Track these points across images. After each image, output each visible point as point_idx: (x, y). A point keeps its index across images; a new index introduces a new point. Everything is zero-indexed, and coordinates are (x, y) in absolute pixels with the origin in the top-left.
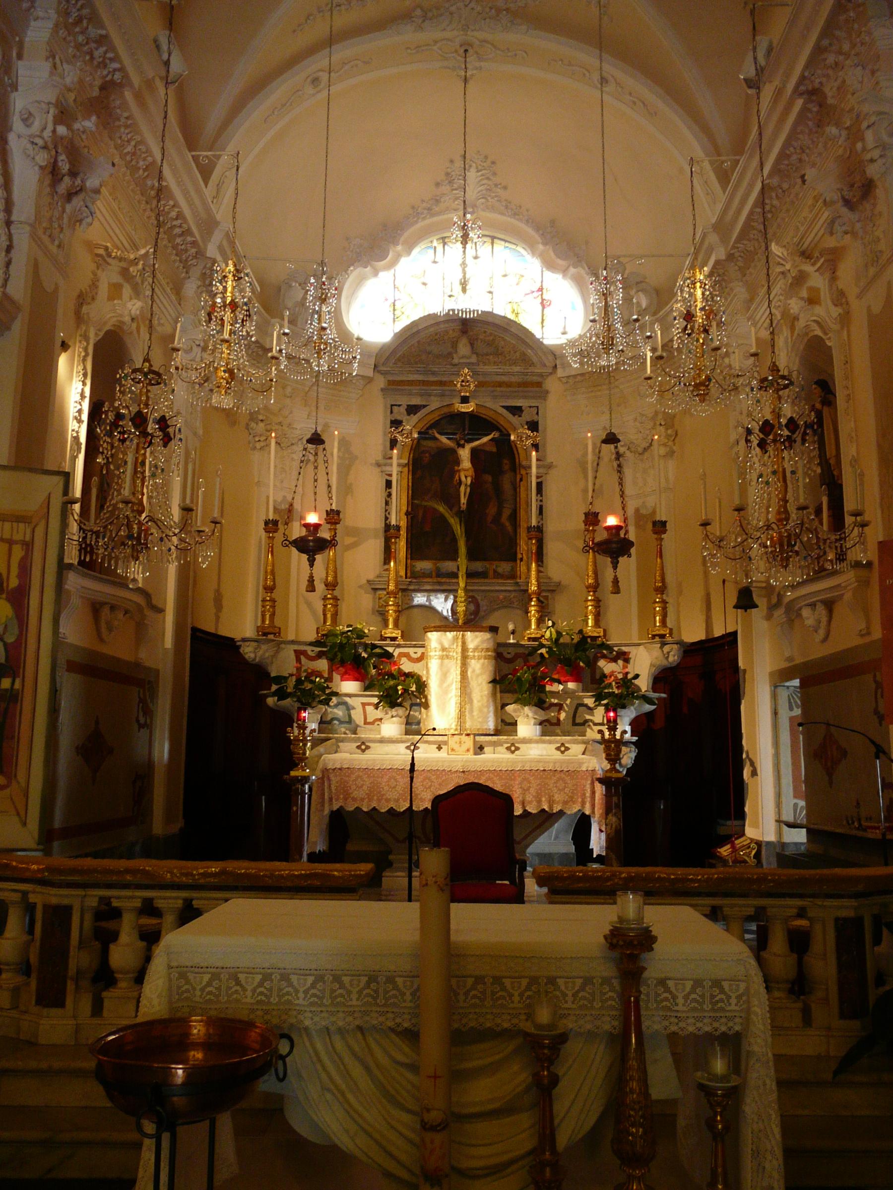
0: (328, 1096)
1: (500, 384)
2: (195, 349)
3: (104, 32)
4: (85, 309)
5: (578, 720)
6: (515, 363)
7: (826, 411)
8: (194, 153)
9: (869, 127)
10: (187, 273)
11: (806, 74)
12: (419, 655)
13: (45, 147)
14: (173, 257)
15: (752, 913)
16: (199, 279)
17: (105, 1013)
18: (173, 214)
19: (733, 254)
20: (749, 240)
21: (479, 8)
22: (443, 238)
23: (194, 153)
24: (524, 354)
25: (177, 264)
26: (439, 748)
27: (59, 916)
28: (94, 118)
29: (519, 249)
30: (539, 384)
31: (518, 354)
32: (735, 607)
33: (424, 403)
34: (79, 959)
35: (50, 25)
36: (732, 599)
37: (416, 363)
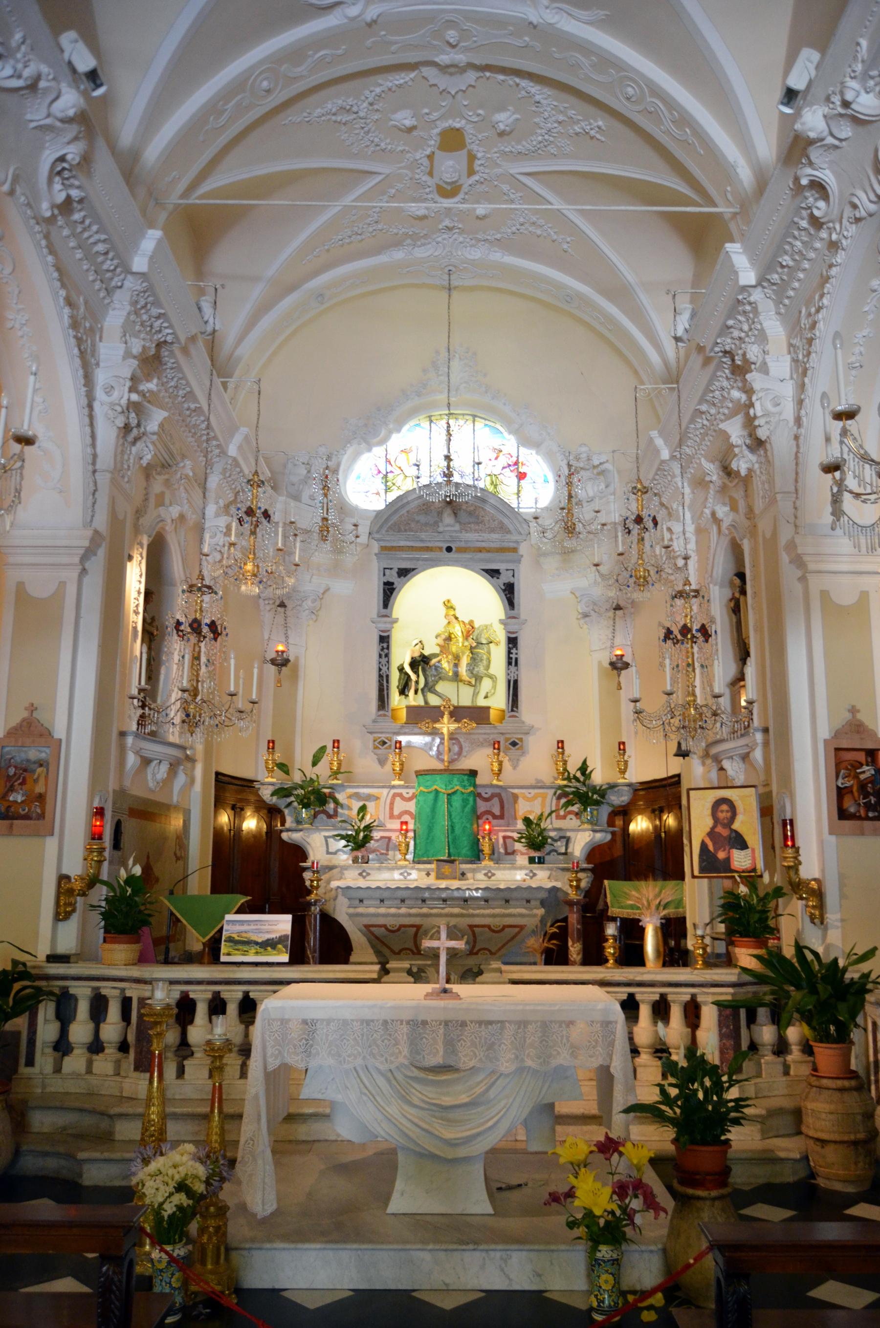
0: (365, 1098)
1: (480, 550)
3: (163, 311)
4: (141, 521)
6: (492, 531)
7: (742, 598)
12: (410, 795)
13: (123, 412)
17: (186, 1076)
21: (461, 239)
22: (430, 417)
24: (501, 523)
26: (428, 874)
28: (155, 381)
29: (498, 426)
30: (515, 550)
32: (676, 755)
35: (125, 313)
37: (406, 531)
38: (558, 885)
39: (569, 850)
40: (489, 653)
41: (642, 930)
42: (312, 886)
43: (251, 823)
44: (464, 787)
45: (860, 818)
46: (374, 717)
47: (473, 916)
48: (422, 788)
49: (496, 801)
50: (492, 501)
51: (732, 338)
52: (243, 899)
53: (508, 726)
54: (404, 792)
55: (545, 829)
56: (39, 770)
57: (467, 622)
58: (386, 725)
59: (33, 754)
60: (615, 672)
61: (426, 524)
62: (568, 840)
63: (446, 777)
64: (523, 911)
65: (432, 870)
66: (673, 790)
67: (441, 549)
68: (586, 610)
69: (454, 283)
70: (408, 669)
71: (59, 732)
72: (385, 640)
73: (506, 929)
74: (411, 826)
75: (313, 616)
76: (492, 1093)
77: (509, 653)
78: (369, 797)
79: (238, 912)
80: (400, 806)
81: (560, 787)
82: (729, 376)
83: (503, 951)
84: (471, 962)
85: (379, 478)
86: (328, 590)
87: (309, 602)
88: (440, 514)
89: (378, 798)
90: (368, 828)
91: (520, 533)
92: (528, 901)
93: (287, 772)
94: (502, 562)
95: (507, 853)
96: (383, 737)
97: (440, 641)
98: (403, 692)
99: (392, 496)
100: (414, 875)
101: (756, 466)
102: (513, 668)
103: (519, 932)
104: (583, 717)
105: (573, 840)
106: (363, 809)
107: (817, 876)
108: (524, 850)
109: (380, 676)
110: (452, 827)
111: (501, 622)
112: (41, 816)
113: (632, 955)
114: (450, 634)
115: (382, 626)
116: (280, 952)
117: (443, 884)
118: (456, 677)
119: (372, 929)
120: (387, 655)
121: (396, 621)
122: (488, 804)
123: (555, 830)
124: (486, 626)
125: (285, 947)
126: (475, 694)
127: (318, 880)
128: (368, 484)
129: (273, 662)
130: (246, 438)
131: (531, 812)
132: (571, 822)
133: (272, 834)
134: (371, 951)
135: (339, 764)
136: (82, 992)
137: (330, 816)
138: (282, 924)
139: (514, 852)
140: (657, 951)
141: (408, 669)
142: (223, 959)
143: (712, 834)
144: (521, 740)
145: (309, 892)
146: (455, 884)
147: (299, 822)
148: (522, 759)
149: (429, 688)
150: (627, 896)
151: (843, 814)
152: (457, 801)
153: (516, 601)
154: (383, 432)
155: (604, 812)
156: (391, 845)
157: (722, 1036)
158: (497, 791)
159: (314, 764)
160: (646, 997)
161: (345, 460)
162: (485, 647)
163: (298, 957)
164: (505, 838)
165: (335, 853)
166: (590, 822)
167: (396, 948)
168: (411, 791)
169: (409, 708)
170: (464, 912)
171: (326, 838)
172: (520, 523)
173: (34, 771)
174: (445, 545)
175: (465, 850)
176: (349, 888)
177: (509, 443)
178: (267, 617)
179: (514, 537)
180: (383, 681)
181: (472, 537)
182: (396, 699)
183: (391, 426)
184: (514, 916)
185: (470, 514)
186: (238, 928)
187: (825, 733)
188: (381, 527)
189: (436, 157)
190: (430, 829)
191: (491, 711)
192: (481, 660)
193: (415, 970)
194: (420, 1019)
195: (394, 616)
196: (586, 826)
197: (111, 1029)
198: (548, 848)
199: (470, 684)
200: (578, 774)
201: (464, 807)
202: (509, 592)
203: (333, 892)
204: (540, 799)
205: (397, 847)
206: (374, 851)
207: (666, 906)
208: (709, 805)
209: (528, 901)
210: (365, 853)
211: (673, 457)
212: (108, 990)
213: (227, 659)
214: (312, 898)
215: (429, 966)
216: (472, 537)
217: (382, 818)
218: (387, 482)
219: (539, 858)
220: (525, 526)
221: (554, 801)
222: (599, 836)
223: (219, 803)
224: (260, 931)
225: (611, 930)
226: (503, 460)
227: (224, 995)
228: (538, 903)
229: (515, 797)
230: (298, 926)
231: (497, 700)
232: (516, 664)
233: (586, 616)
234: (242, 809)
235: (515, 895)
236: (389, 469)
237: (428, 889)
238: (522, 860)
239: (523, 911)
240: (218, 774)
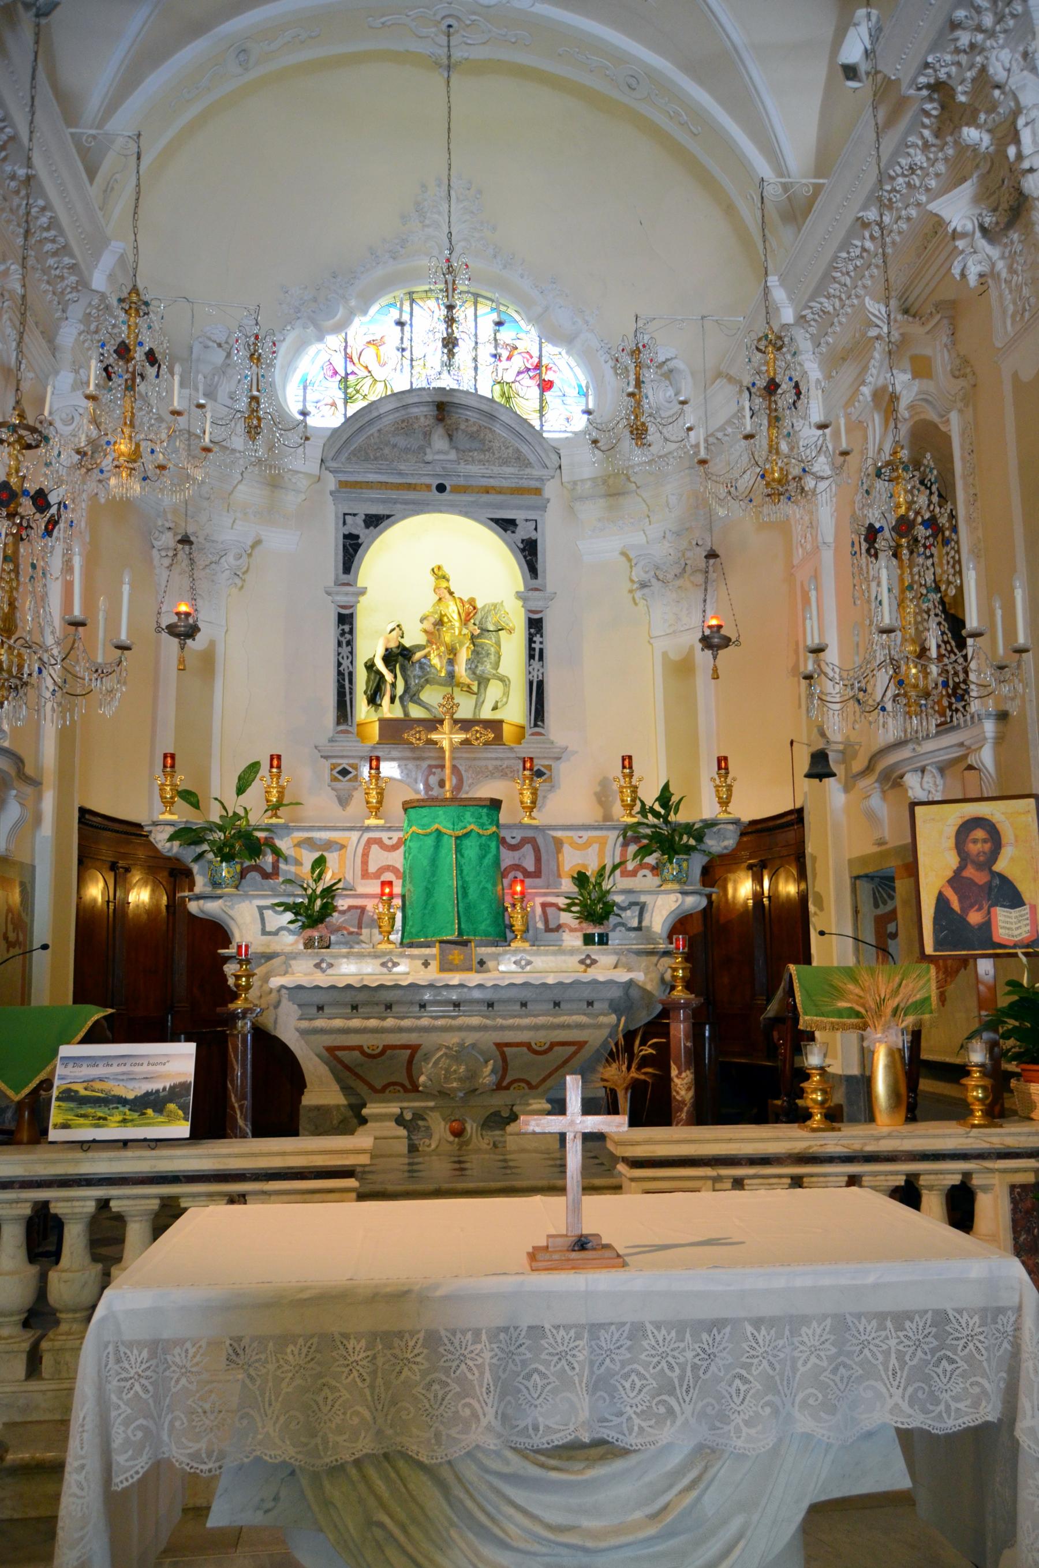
1: (487, 490)
2: (77, 418)
5: (552, 925)
6: (505, 462)
8: (73, 130)
9: (1027, 124)
10: (64, 311)
11: (930, 60)
12: (394, 841)
14: (44, 286)
15: (903, 1183)
16: (81, 321)
18: (44, 220)
19: (804, 317)
20: (828, 297)
22: (411, 293)
23: (73, 130)
24: (518, 450)
25: (50, 296)
26: (426, 964)
30: (538, 491)
31: (510, 450)
32: (808, 776)
33: (387, 513)
36: (804, 764)
37: (376, 459)
38: (639, 976)
39: (644, 924)
40: (498, 644)
42: (237, 986)
43: (140, 896)
44: (482, 825)
46: (331, 734)
47: (502, 1028)
48: (414, 828)
49: (528, 848)
51: (957, 51)
53: (529, 748)
54: (384, 836)
55: (608, 892)
57: (465, 599)
58: (349, 746)
60: (709, 653)
61: (407, 450)
62: (642, 908)
63: (452, 810)
65: (434, 957)
66: (790, 835)
67: (428, 487)
68: (645, 577)
69: (457, 54)
70: (380, 665)
72: (346, 620)
73: (556, 1048)
74: (397, 889)
75: (238, 581)
77: (531, 641)
78: (329, 845)
79: (89, 1039)
80: (378, 858)
82: (931, 140)
83: (549, 1083)
84: (498, 1101)
85: (334, 383)
86: (258, 543)
87: (231, 558)
88: (427, 435)
89: (343, 847)
92: (590, 1004)
93: (196, 805)
94: (519, 507)
95: (548, 930)
96: (344, 763)
97: (428, 625)
98: (373, 700)
99: (353, 409)
101: (1000, 265)
102: (536, 663)
103: (575, 1053)
105: (650, 907)
106: (320, 863)
108: (574, 923)
109: (340, 674)
110: (464, 890)
114: (442, 616)
115: (342, 599)
116: (171, 1118)
117: (455, 979)
119: (339, 1053)
120: (349, 643)
122: (517, 854)
123: (623, 892)
124: (495, 606)
125: (183, 1107)
126: (478, 705)
127: (249, 976)
128: (317, 385)
129: (172, 630)
130: (122, 259)
132: (646, 880)
133: (175, 907)
134: (336, 1087)
135: (281, 794)
137: (266, 876)
138: (176, 1061)
139: (559, 928)
141: (380, 665)
142: (54, 1135)
143: (956, 881)
145: (234, 996)
146: (473, 979)
147: (215, 884)
148: (550, 796)
152: (471, 849)
153: (540, 567)
154: (341, 313)
155: (697, 862)
156: (365, 919)
158: (530, 834)
159: (240, 790)
161: (283, 349)
162: (493, 635)
163: (210, 1122)
164: (544, 905)
165: (276, 933)
166: (677, 880)
167: (378, 1084)
168: (396, 836)
169: (384, 723)
170: (488, 1022)
171: (261, 909)
172: (545, 450)
175: (485, 925)
176: (300, 987)
178: (161, 562)
179: (536, 472)
181: (474, 471)
182: (362, 710)
183: (353, 303)
184: (568, 1027)
185: (472, 437)
186: (86, 1071)
188: (339, 452)
191: (505, 726)
192: (488, 654)
193: (408, 1116)
194: (525, 1323)
195: (361, 583)
198: (613, 920)
199: (469, 690)
200: (657, 807)
201: (482, 857)
202: (529, 553)
203: (274, 995)
204: (596, 846)
205: (376, 923)
206: (338, 929)
208: (951, 831)
209: (590, 1004)
210: (325, 932)
211: (801, 319)
214: (239, 1005)
215: (432, 1109)
216: (474, 471)
217: (349, 877)
218: (346, 387)
219: (600, 935)
220: (555, 457)
221: (618, 850)
223: (86, 861)
226: (518, 362)
227: (55, 1209)
228: (605, 1006)
229: (559, 844)
230: (211, 1069)
231: (514, 711)
232: (541, 658)
233: (643, 585)
234: (127, 870)
236: (350, 368)
237: (431, 986)
238: (573, 940)
240: (83, 811)
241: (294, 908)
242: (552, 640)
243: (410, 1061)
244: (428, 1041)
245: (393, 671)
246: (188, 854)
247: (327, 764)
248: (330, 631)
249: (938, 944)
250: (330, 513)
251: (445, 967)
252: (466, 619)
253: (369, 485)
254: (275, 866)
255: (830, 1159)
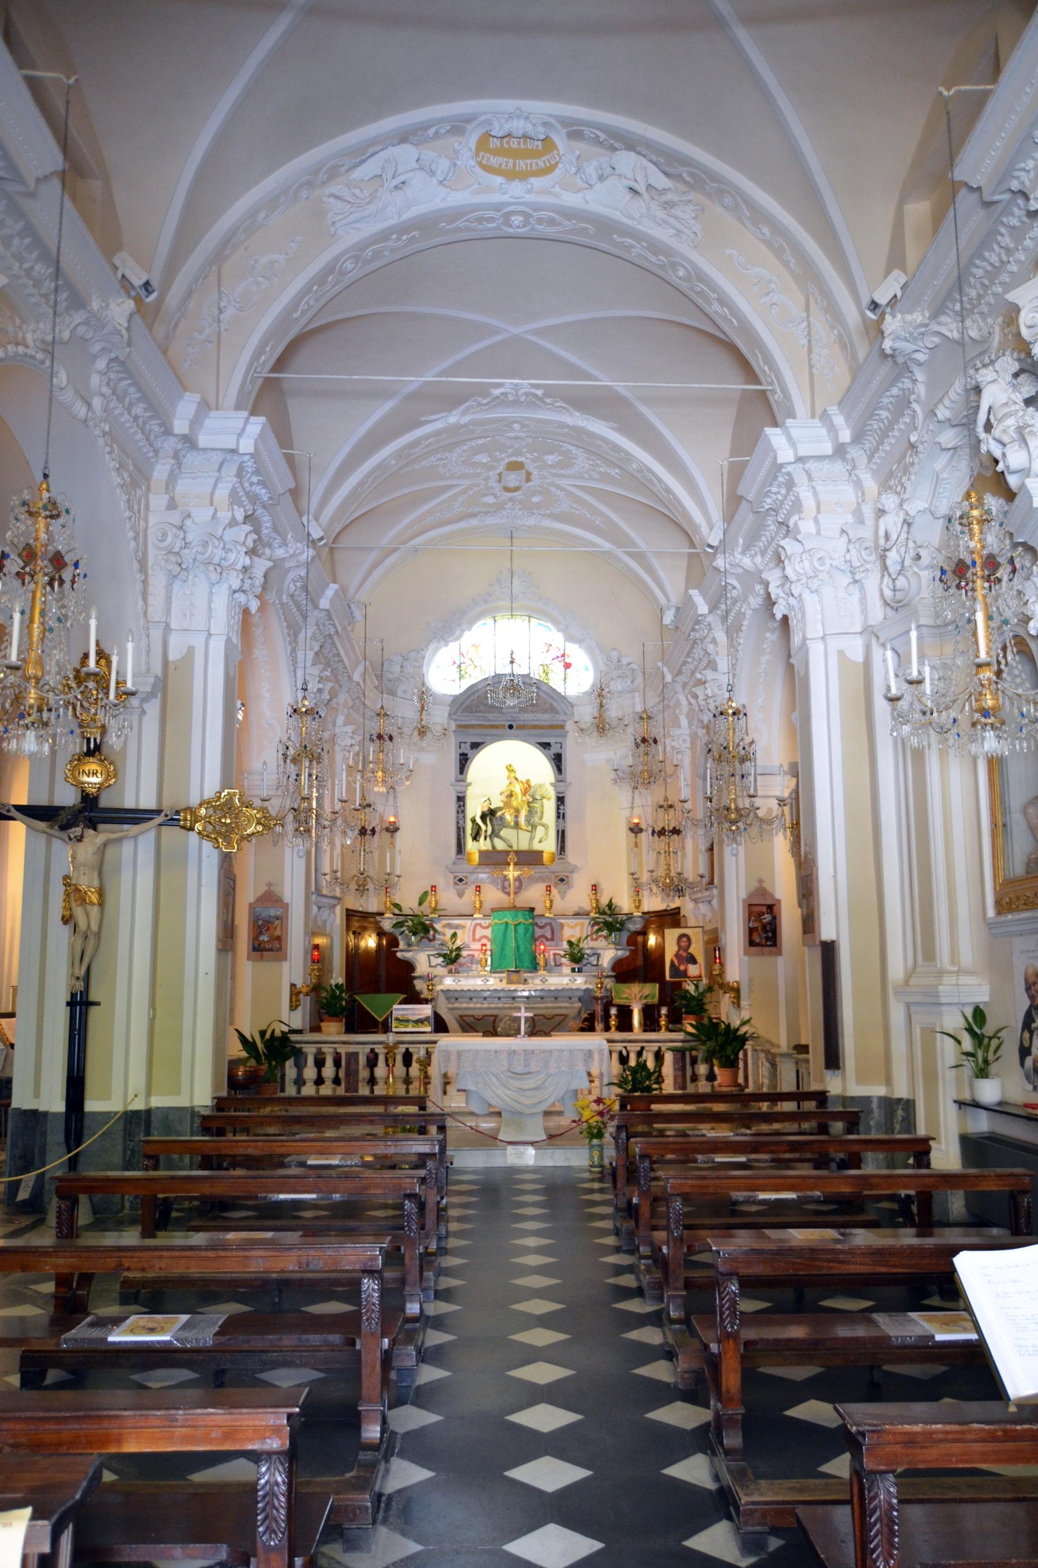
1: (535, 727)
6: (545, 712)
24: (552, 705)
27: (353, 1057)
29: (549, 625)
30: (562, 727)
34: (364, 1074)
38: (591, 987)
40: (542, 806)
41: (632, 1011)
45: (762, 946)
49: (548, 928)
50: (544, 688)
52: (402, 997)
53: (557, 866)
54: (482, 922)
56: (277, 922)
59: (272, 912)
62: (599, 955)
63: (512, 913)
64: (567, 1005)
67: (504, 726)
70: (479, 821)
71: (287, 899)
72: (461, 799)
74: (489, 947)
76: (547, 1084)
77: (558, 809)
78: (458, 927)
79: (400, 1003)
80: (480, 932)
81: (594, 919)
90: (459, 949)
91: (566, 714)
94: (551, 736)
95: (556, 965)
96: (461, 876)
97: (503, 798)
98: (476, 838)
99: (466, 684)
100: (491, 981)
104: (611, 868)
106: (454, 935)
107: (737, 979)
108: (568, 963)
109: (458, 828)
111: (552, 784)
112: (280, 949)
113: (625, 1024)
115: (459, 789)
117: (512, 987)
118: (517, 825)
121: (470, 784)
124: (540, 786)
126: (532, 839)
131: (573, 936)
132: (601, 943)
136: (310, 1051)
137: (430, 940)
139: (561, 965)
140: (640, 1024)
141: (479, 821)
143: (677, 955)
144: (567, 877)
147: (409, 945)
149: (495, 834)
150: (624, 992)
151: (752, 943)
152: (521, 930)
153: (563, 768)
154: (458, 632)
155: (625, 936)
157: (675, 1069)
158: (549, 921)
160: (633, 1049)
161: (428, 654)
164: (554, 954)
166: (614, 943)
169: (481, 852)
171: (429, 956)
173: (273, 923)
174: (508, 724)
175: (527, 963)
177: (557, 638)
180: (460, 831)
182: (470, 845)
186: (402, 1013)
187: (743, 895)
189: (503, 476)
190: (502, 949)
191: (545, 855)
195: (469, 780)
196: (611, 946)
197: (329, 1071)
198: (584, 961)
202: (558, 760)
205: (479, 962)
207: (646, 997)
208: (676, 938)
212: (327, 1049)
213: (88, 618)
222: (620, 953)
224: (414, 1014)
225: (613, 1011)
229: (562, 926)
231: (548, 845)
235: (561, 994)
237: (503, 990)
238: (566, 970)
239: (567, 1005)
241: (444, 956)
242: (569, 808)
243: (494, 1022)
244: (501, 1013)
245: (485, 823)
246: (396, 932)
247: (452, 876)
248: (453, 805)
249: (671, 977)
250: (452, 741)
251: (510, 982)
252: (525, 792)
253: (472, 726)
254: (434, 936)
255: (617, 1042)
